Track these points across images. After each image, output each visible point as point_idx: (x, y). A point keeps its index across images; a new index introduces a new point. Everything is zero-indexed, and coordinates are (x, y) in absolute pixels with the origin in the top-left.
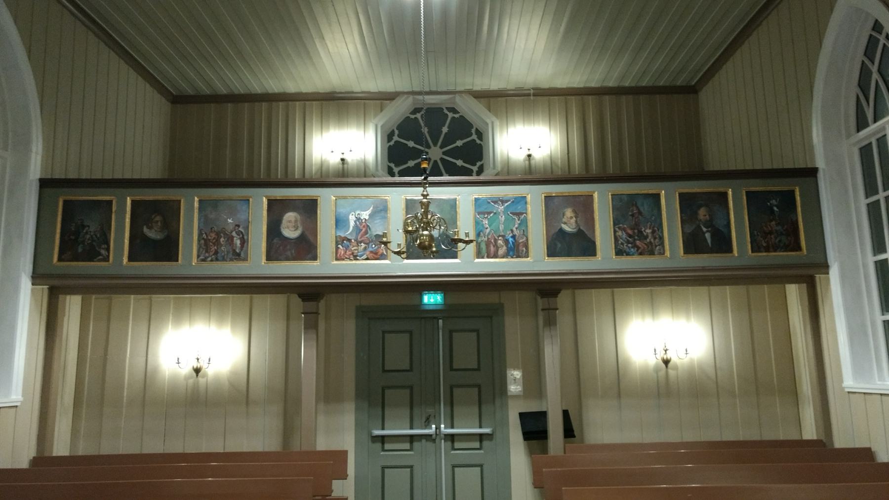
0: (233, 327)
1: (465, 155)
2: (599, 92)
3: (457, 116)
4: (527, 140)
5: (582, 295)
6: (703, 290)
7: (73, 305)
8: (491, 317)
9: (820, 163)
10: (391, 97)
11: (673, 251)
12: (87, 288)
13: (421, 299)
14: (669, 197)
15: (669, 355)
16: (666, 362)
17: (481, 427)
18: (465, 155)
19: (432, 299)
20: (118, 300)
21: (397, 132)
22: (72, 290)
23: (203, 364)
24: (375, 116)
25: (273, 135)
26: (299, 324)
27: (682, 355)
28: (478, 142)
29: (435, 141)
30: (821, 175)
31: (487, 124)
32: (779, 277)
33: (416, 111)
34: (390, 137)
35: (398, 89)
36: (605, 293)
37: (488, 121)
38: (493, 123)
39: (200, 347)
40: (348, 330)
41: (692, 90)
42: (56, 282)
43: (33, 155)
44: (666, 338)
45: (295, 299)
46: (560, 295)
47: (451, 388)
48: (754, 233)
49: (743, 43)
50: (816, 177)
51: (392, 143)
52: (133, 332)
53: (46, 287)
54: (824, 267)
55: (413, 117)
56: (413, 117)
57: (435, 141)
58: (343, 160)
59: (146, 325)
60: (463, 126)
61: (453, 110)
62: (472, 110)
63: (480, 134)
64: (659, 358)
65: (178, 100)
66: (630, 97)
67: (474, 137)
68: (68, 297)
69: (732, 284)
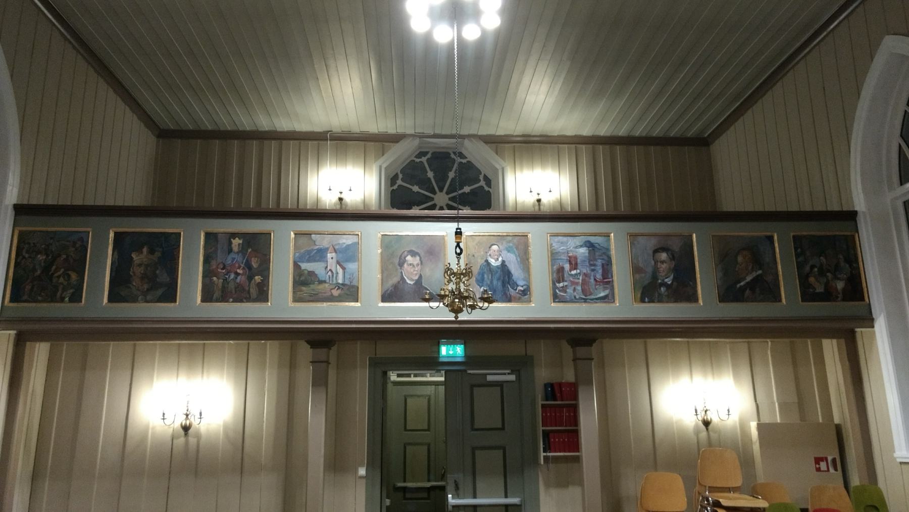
0: (736, 376)
1: (474, 195)
2: (610, 141)
3: (464, 161)
4: (539, 184)
5: (609, 345)
6: (741, 344)
7: (40, 352)
8: (519, 371)
9: (859, 203)
10: (396, 139)
11: (705, 303)
12: (56, 333)
13: (438, 352)
14: (700, 239)
15: (710, 416)
16: (707, 423)
17: (506, 497)
18: (474, 195)
19: (452, 351)
20: (94, 346)
21: (401, 176)
22: (40, 336)
23: (194, 421)
24: (377, 158)
25: (265, 169)
26: (305, 374)
27: (724, 416)
28: (486, 188)
29: (440, 178)
30: (861, 220)
31: (497, 170)
32: (816, 330)
33: (422, 154)
34: (393, 180)
35: (400, 131)
36: (638, 343)
37: (497, 166)
38: (503, 169)
39: (186, 399)
40: (360, 381)
41: (702, 142)
42: (24, 327)
43: (9, 188)
44: (703, 397)
45: (305, 352)
46: (594, 345)
47: (474, 449)
48: (790, 283)
49: (728, 128)
50: (856, 221)
51: (395, 187)
52: (112, 385)
53: (13, 332)
54: (868, 320)
55: (418, 160)
56: (418, 160)
57: (440, 178)
58: (341, 199)
59: (129, 373)
60: (469, 172)
61: (461, 155)
62: (477, 153)
63: (488, 181)
64: (700, 419)
65: (164, 134)
66: (641, 147)
67: (482, 183)
68: (37, 345)
69: (774, 337)
